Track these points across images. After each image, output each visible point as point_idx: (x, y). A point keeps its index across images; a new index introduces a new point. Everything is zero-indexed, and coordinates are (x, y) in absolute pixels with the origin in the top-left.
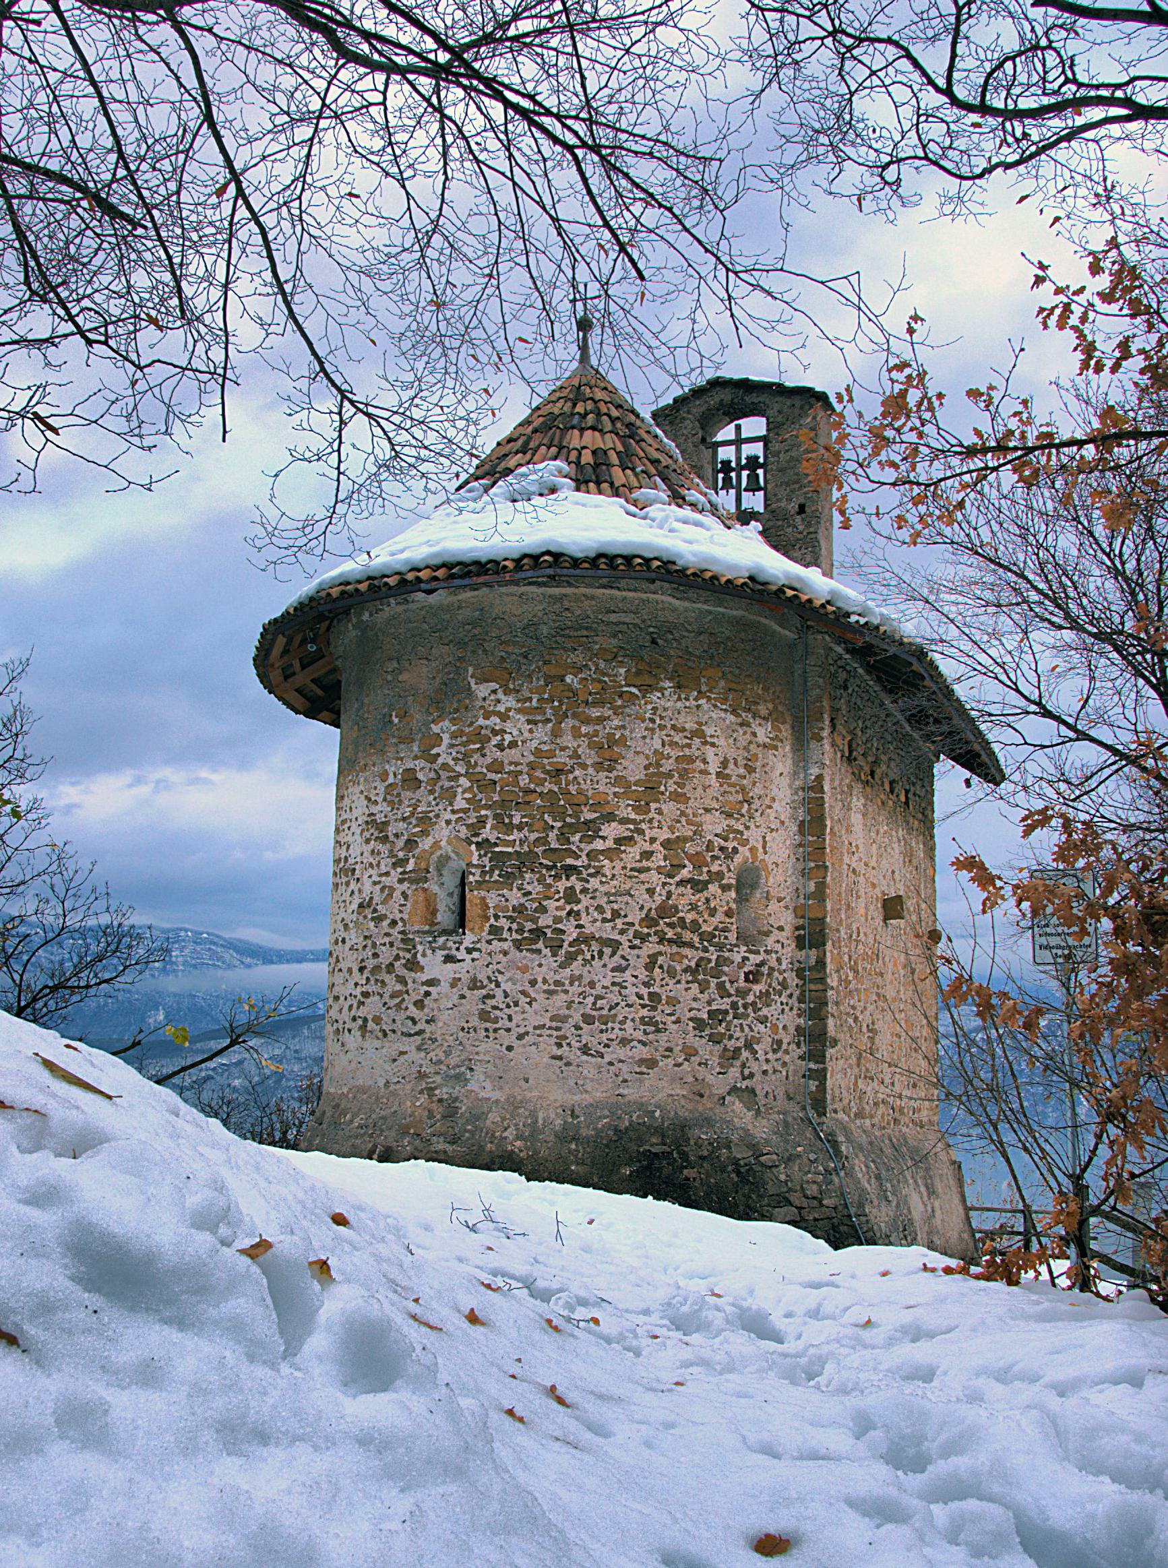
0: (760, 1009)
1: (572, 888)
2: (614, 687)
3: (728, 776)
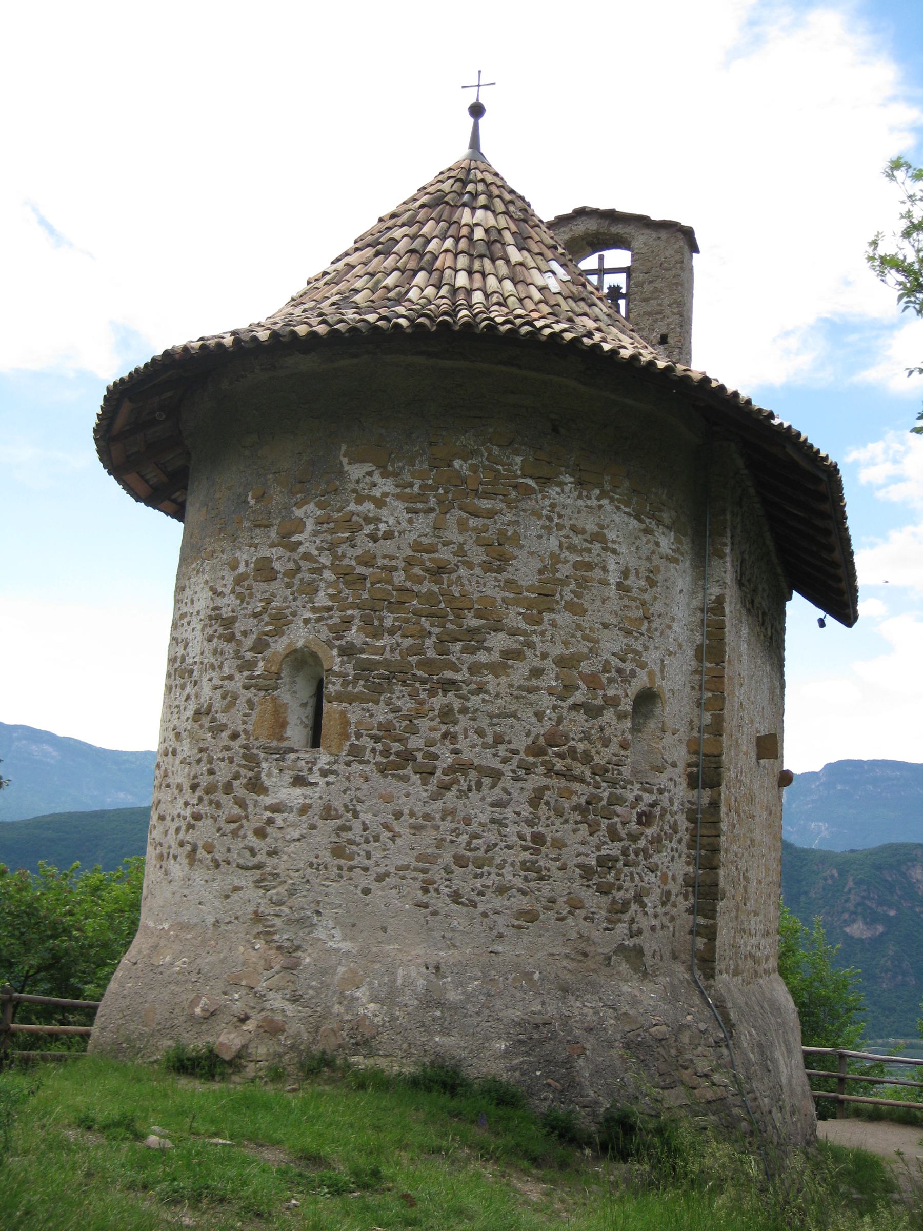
0: (651, 856)
2: (507, 477)
3: (628, 590)
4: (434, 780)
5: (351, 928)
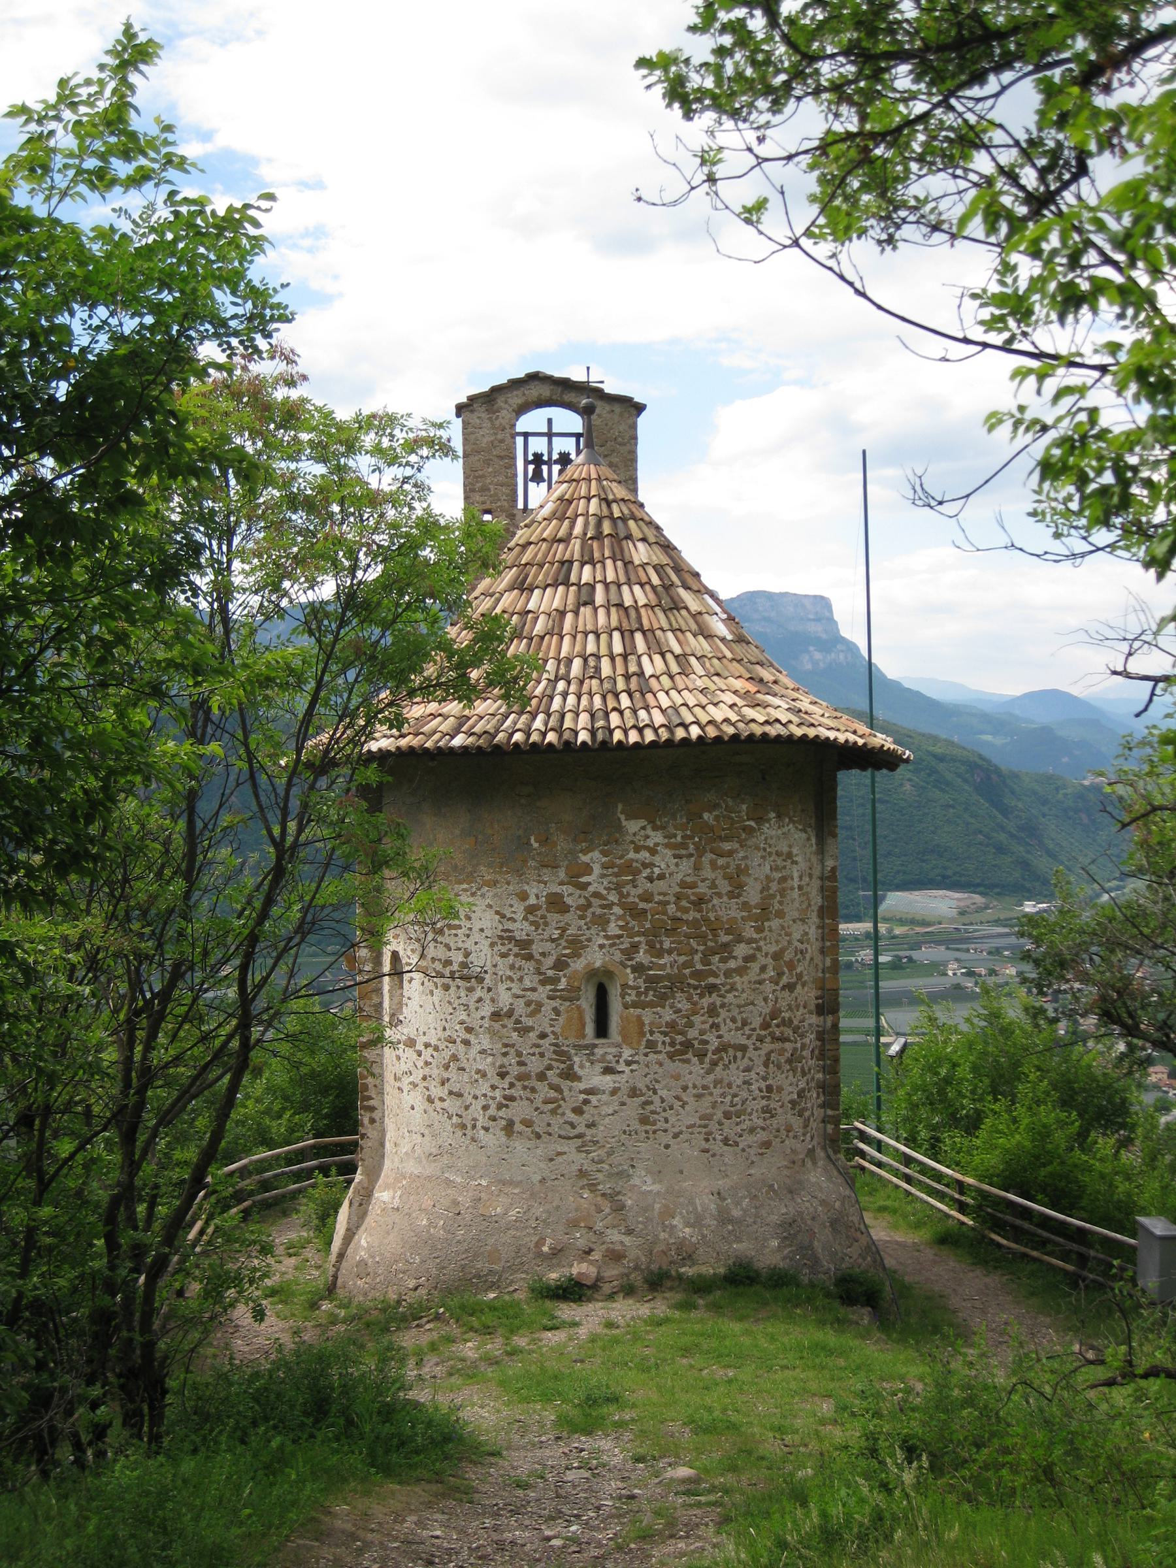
1: (713, 1004)
4: (707, 1060)
5: (658, 1174)
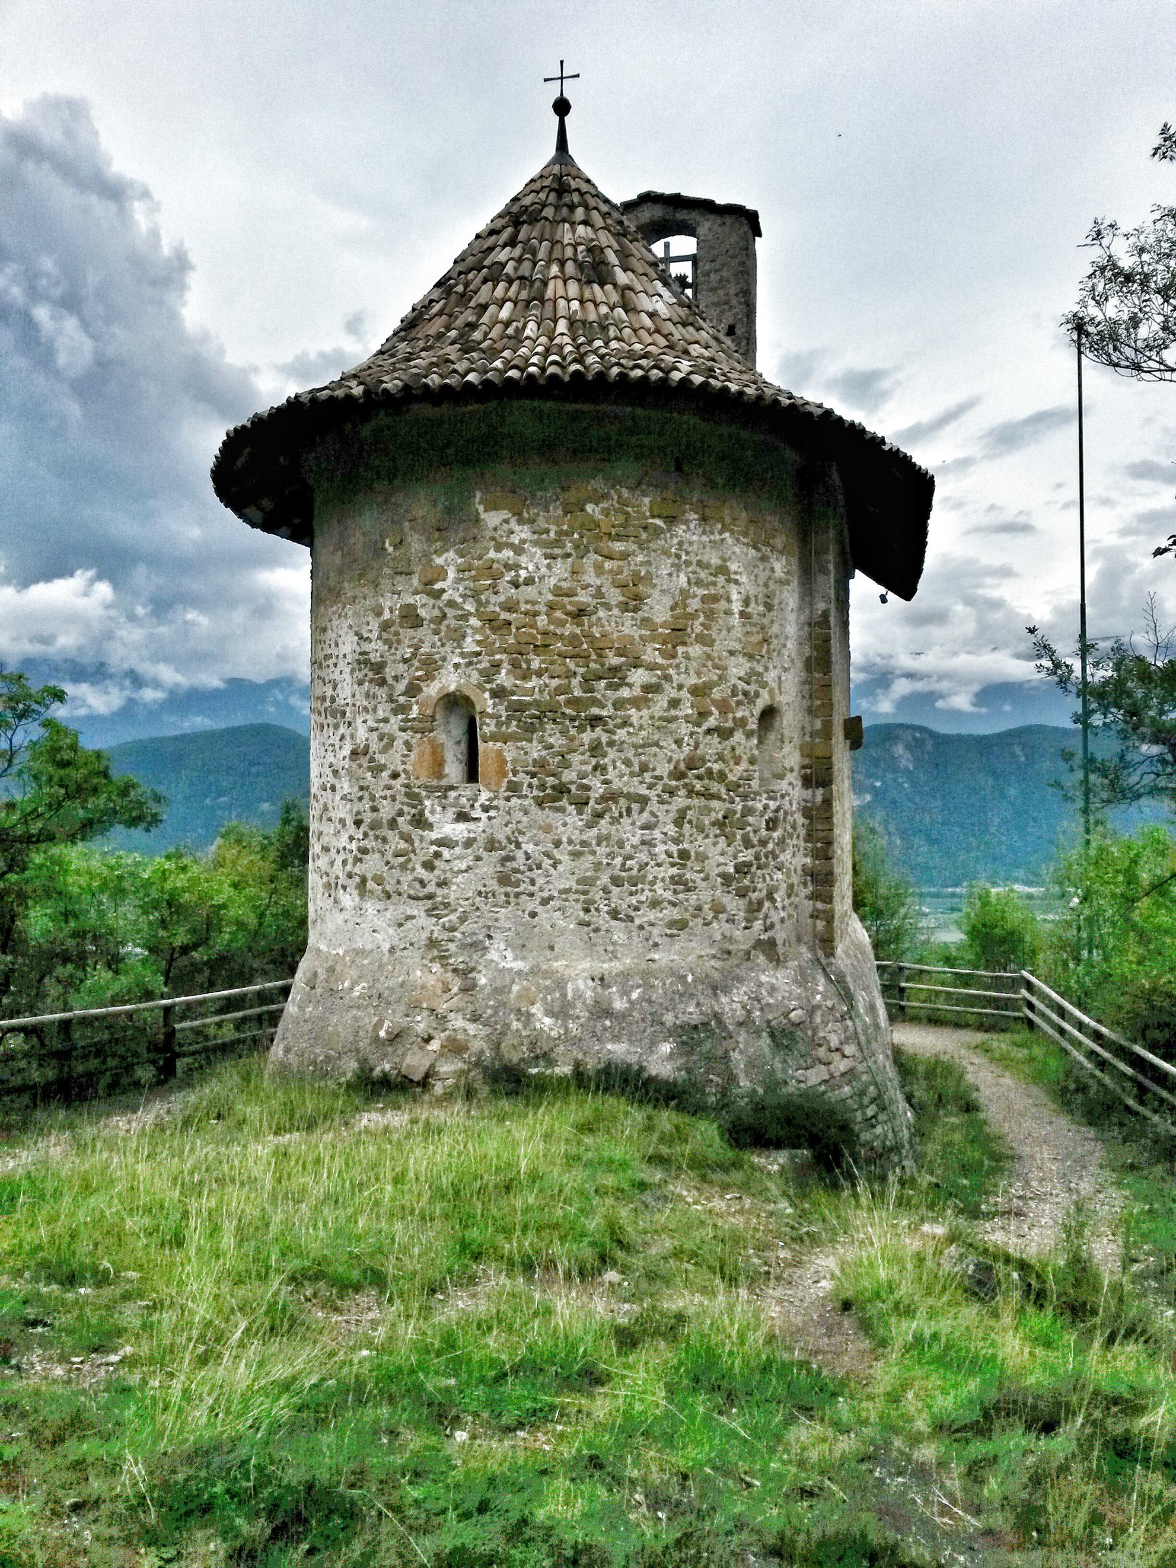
4: (588, 810)
5: (521, 948)
